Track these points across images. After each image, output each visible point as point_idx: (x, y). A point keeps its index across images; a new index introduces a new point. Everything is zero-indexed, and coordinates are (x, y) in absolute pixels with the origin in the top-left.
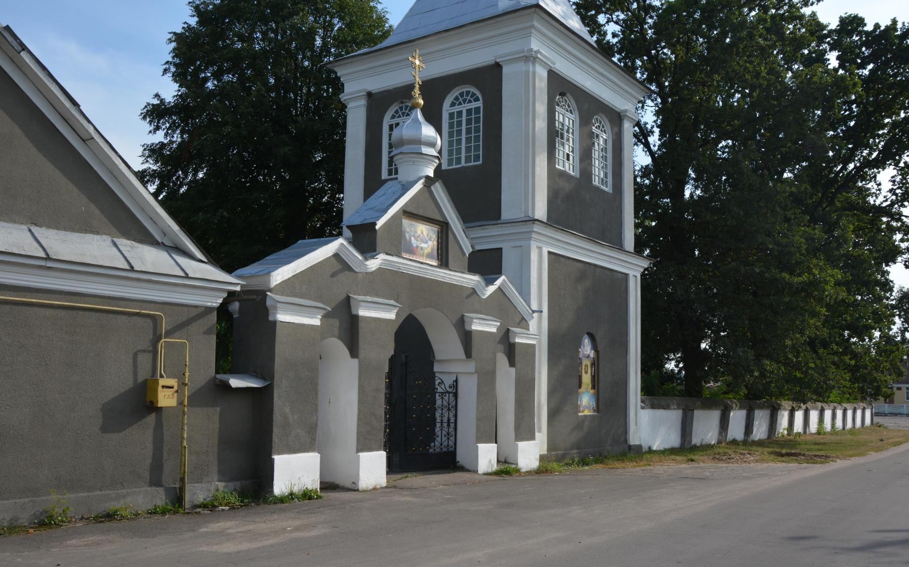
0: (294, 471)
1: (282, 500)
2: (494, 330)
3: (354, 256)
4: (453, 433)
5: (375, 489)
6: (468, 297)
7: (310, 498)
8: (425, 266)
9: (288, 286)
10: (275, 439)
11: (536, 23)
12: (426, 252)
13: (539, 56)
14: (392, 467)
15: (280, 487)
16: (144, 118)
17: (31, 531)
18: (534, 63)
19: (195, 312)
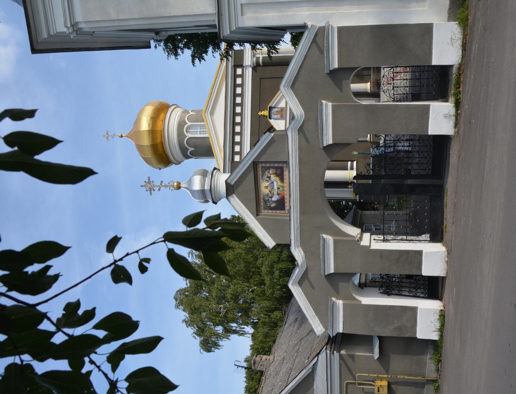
0: (426, 329)
1: (441, 336)
2: (330, 104)
3: (297, 273)
4: (411, 294)
5: (447, 262)
6: (307, 141)
7: (465, 44)
8: (292, 204)
9: (324, 324)
10: (408, 335)
11: (45, 35)
12: (280, 184)
13: (69, 25)
14: (443, 96)
15: (435, 337)
16: (176, 54)
17: (459, 112)
18: (77, 23)
19: (343, 365)
